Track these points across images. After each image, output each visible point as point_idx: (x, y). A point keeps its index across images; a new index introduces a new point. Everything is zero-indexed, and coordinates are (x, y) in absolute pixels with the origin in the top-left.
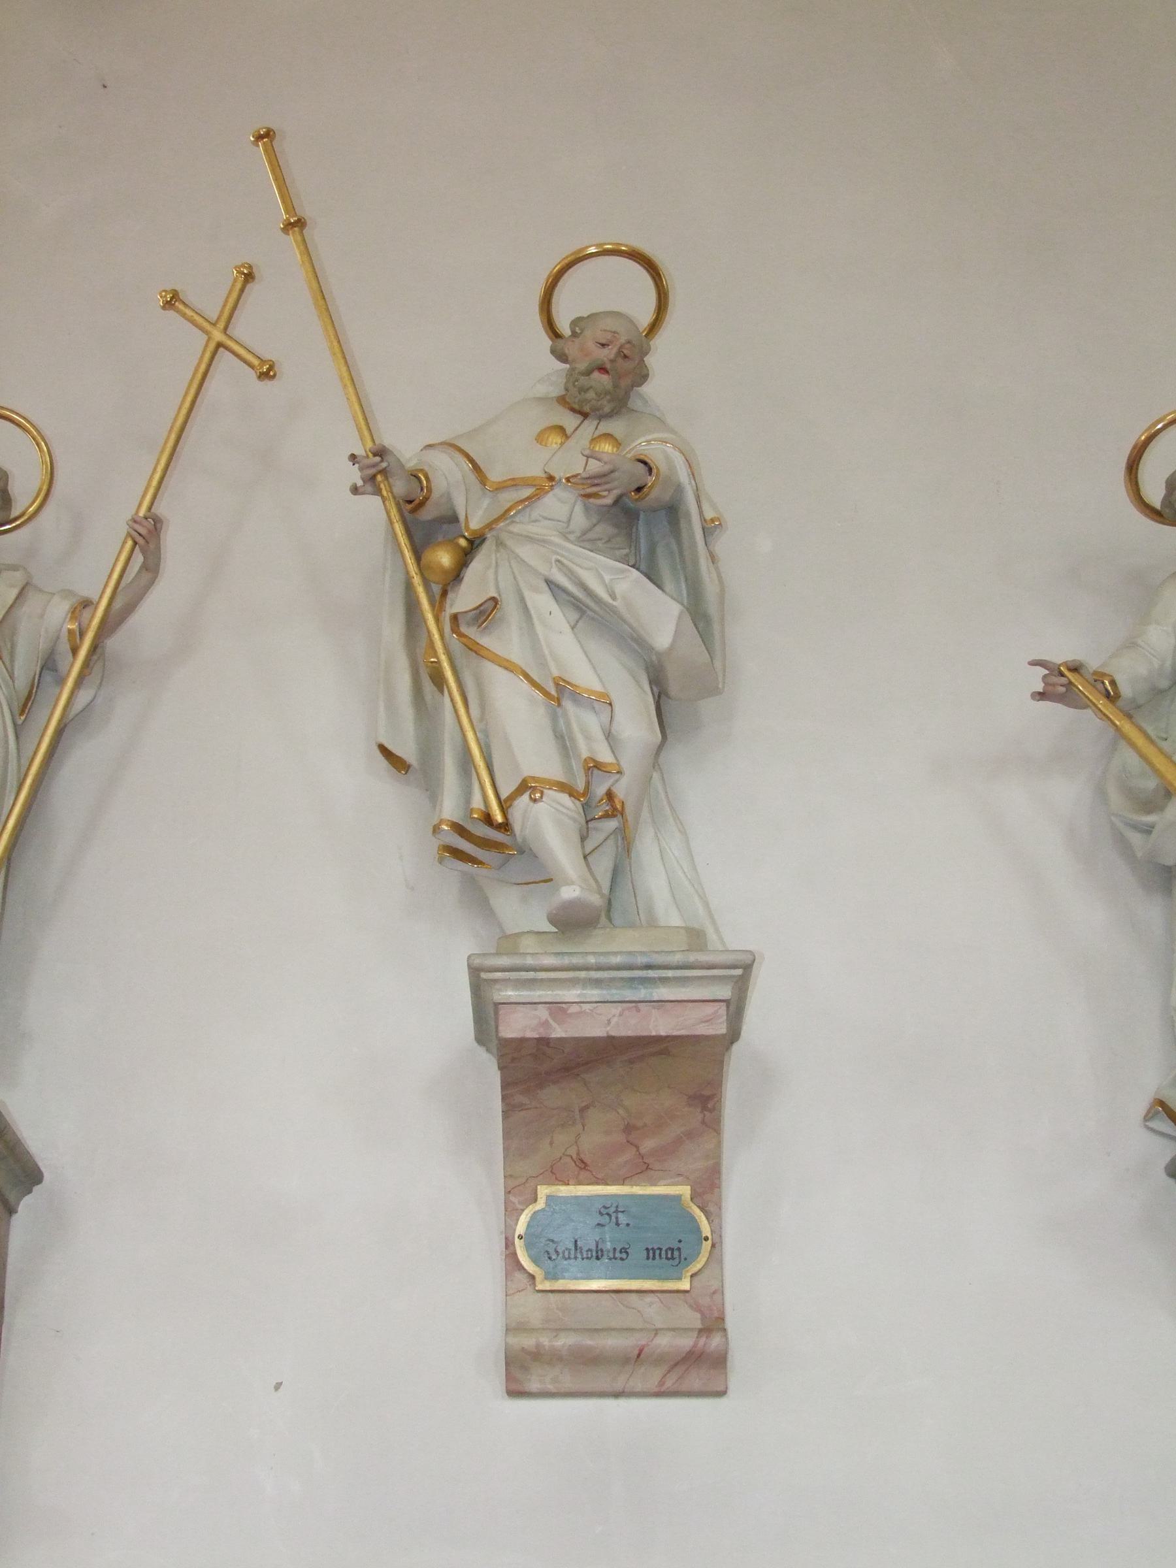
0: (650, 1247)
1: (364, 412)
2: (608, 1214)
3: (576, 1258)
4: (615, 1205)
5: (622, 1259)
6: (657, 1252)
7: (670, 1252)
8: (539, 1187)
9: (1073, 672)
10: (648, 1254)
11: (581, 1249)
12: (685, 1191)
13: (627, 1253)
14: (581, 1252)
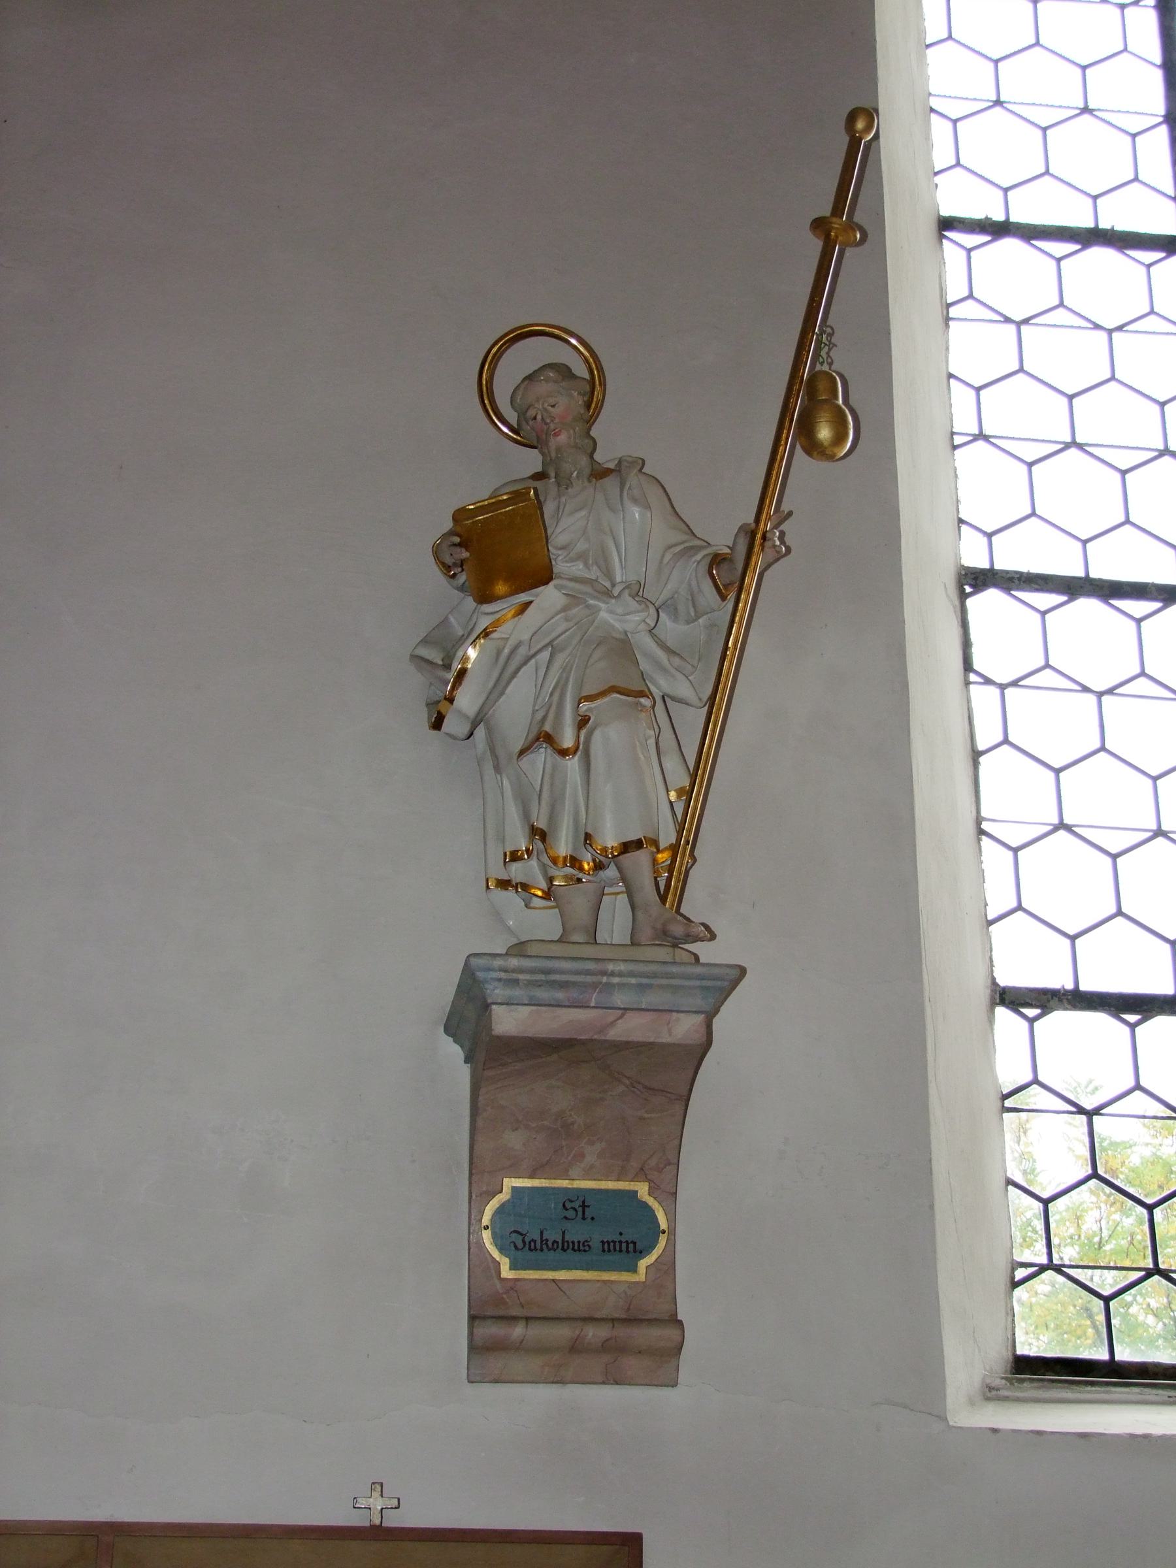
0: (605, 1240)
1: (1047, 48)
3: (542, 1250)
4: (581, 1199)
5: (585, 1251)
6: (576, 1247)
7: (532, 1244)
8: (504, 1179)
9: (971, 750)
10: (603, 1246)
11: (547, 1240)
13: (589, 1246)
14: (546, 1244)
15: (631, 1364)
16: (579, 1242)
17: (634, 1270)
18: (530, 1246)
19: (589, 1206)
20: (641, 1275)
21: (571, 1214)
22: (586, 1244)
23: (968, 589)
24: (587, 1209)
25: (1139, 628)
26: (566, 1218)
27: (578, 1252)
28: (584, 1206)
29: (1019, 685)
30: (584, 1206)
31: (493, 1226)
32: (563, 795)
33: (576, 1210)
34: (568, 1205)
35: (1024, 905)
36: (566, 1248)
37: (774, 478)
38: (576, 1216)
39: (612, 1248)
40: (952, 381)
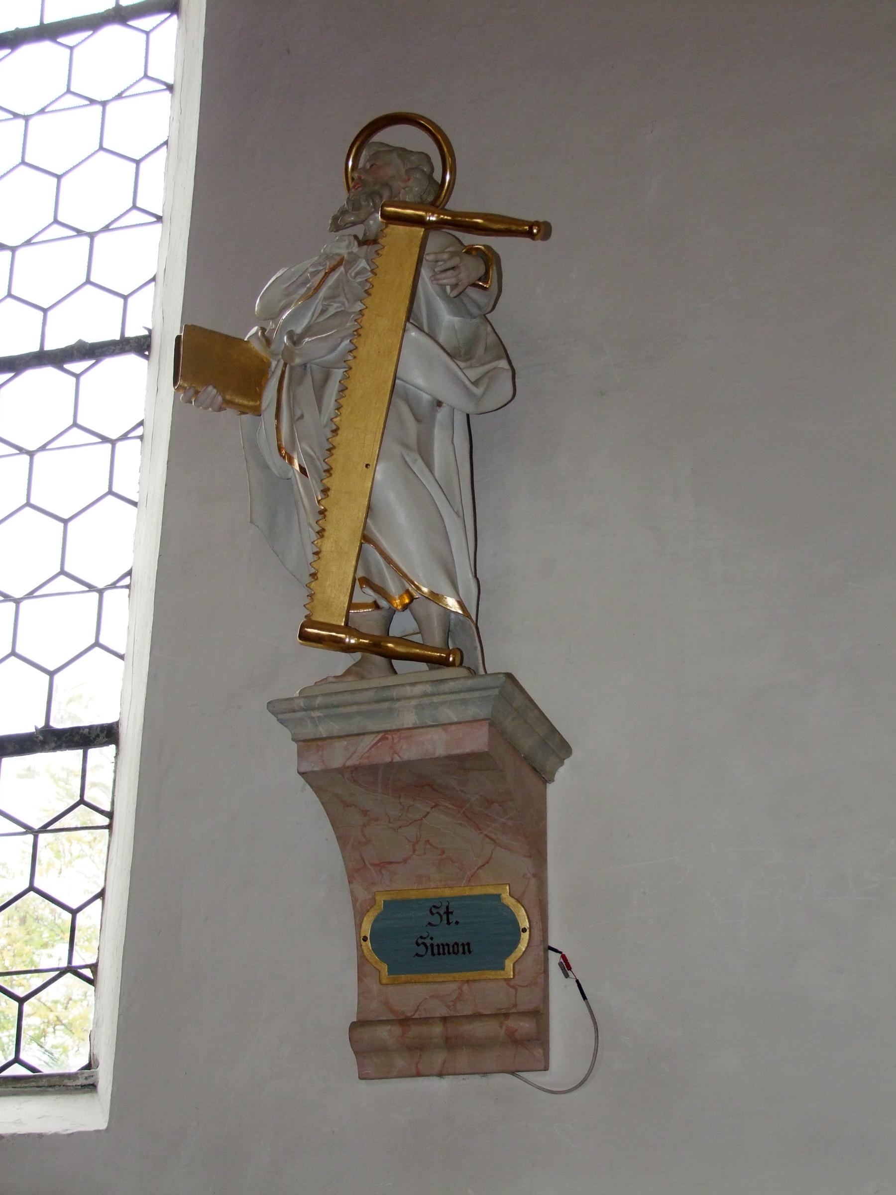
2: (438, 913)
15: (463, 1058)
21: (436, 920)
23: (147, 353)
24: (450, 916)
25: (80, 909)
26: (417, 955)
29: (111, 229)
30: (448, 913)
31: (516, 932)
34: (434, 911)
35: (58, 570)
36: (456, 946)
38: (427, 951)
39: (446, 951)
40: (107, 808)
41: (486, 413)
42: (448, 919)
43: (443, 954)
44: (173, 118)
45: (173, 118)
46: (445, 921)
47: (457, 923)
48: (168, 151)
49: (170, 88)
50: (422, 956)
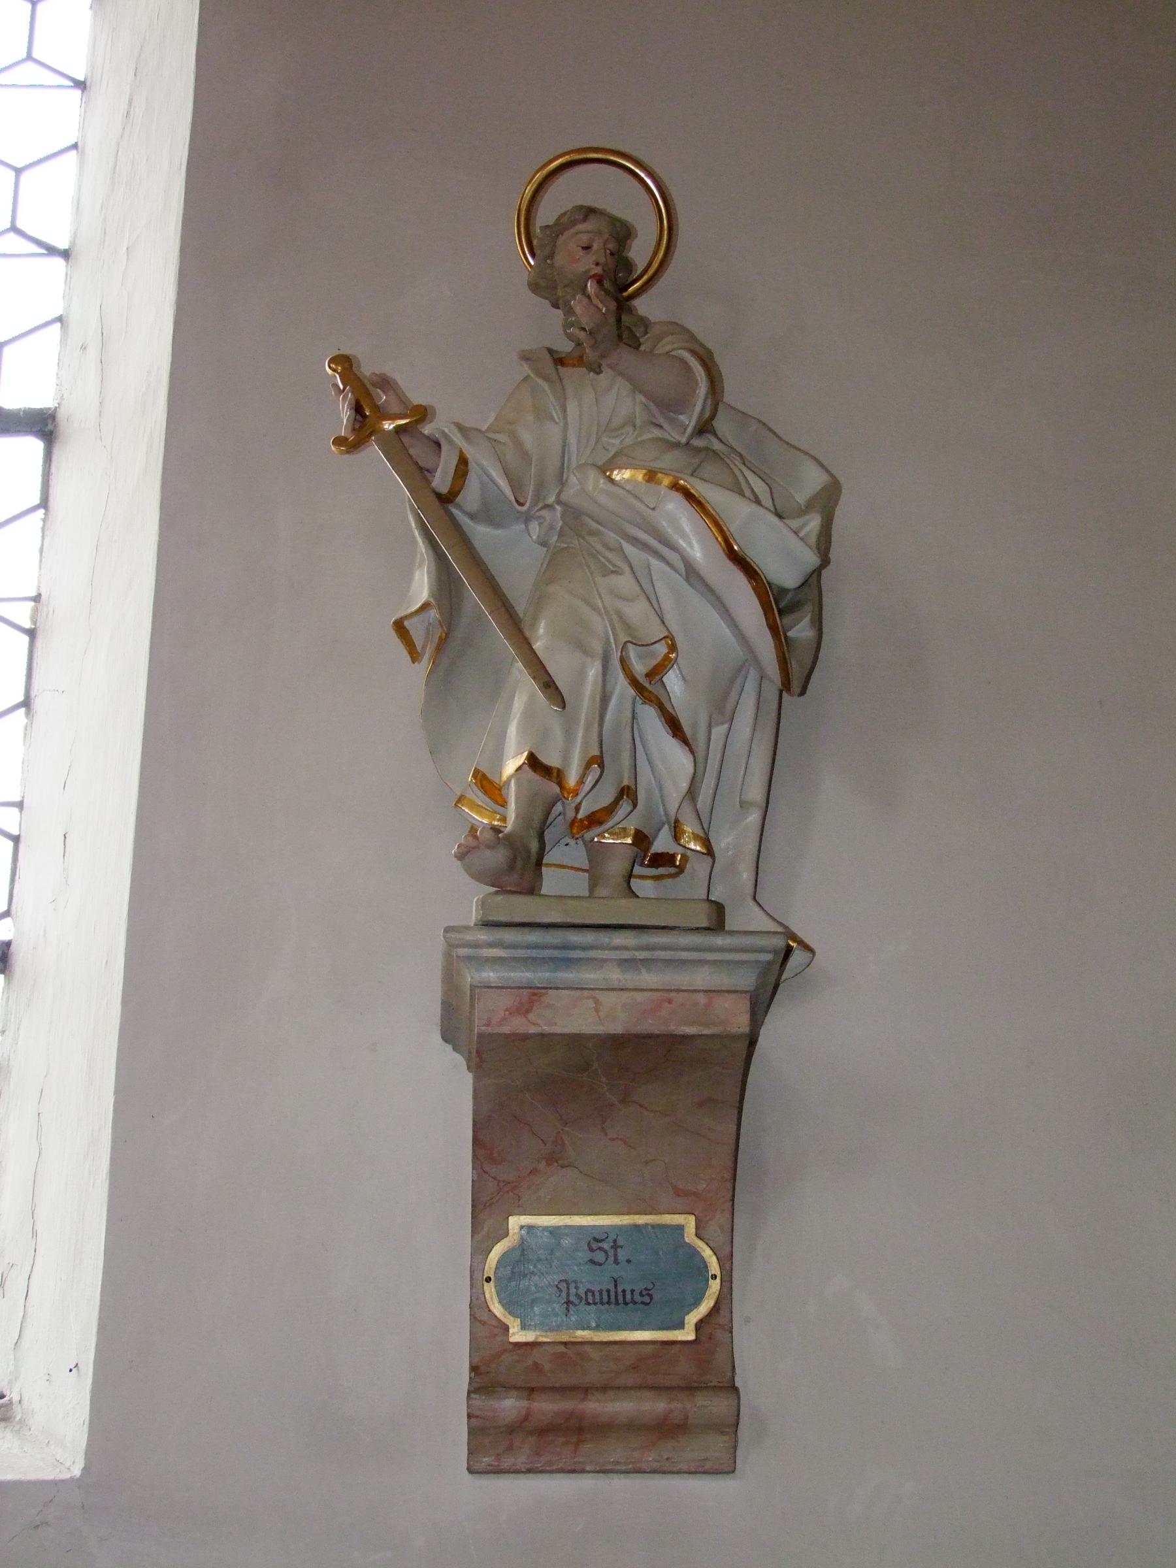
12: (689, 1223)
13: (651, 1296)
16: (632, 1291)
17: (681, 1325)
18: (587, 1300)
19: (622, 1247)
20: (687, 1334)
22: (644, 1293)
24: (619, 1250)
26: (592, 1261)
27: (593, 1305)
28: (615, 1246)
32: (611, 693)
33: (606, 1252)
37: (526, 249)
41: (756, 881)
42: (616, 1256)
43: (603, 1290)
44: (54, 611)
45: (54, 611)
46: (611, 1259)
47: (629, 1261)
48: (64, 341)
49: (81, 85)
50: (600, 1265)
